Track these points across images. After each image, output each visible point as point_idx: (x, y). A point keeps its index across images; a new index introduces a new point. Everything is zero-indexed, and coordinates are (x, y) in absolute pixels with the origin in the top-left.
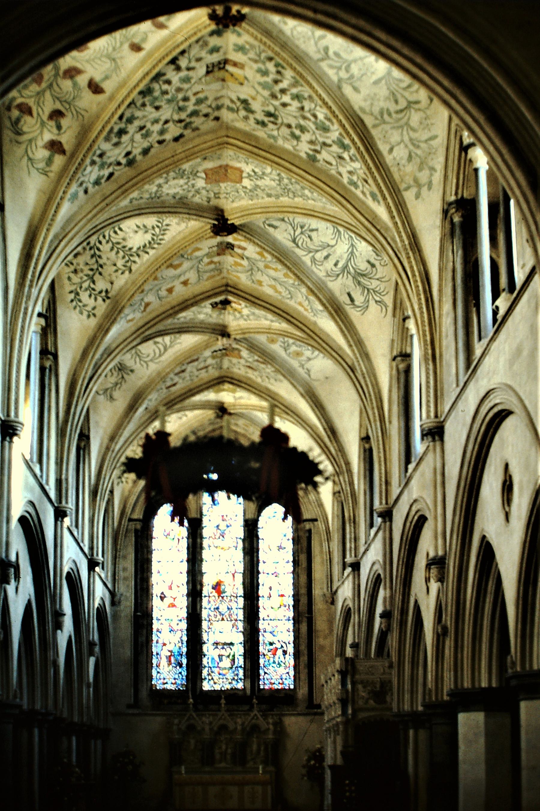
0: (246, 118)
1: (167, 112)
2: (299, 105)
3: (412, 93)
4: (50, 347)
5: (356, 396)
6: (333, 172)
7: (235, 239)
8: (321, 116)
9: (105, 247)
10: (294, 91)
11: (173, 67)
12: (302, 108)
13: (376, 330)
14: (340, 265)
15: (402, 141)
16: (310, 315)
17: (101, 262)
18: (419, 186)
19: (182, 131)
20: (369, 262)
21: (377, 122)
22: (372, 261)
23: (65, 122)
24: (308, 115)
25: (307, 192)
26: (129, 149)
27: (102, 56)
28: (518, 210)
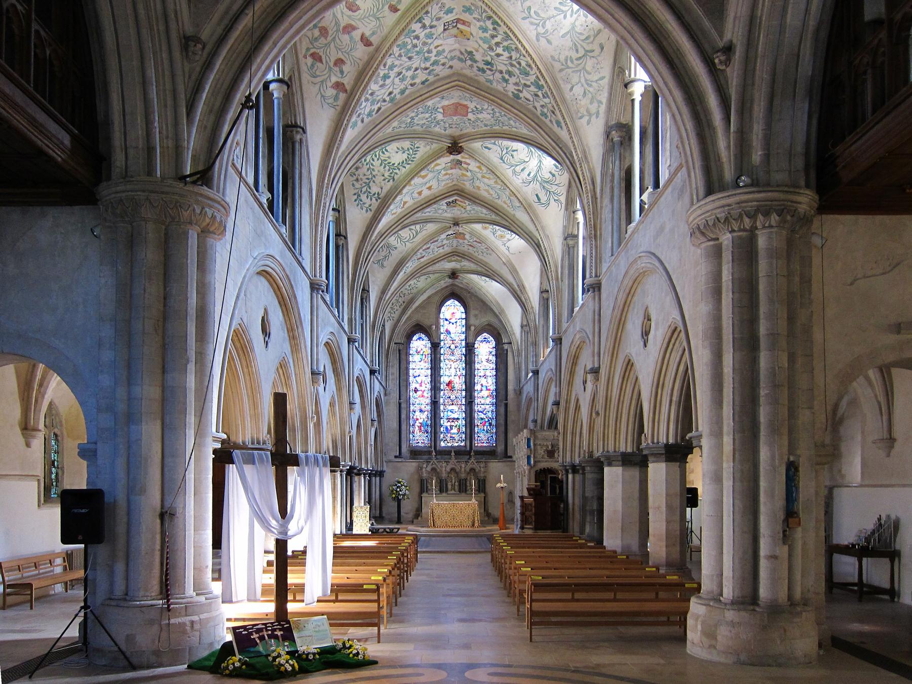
0: (471, 66)
1: (416, 63)
4: (343, 232)
5: (539, 264)
6: (530, 107)
7: (463, 157)
8: (523, 64)
10: (505, 44)
11: (420, 25)
12: (511, 58)
13: (553, 220)
15: (580, 81)
16: (510, 210)
17: (374, 173)
18: (590, 115)
20: (550, 173)
22: (553, 172)
23: (346, 68)
24: (514, 63)
25: (511, 122)
26: (391, 90)
28: (673, 123)
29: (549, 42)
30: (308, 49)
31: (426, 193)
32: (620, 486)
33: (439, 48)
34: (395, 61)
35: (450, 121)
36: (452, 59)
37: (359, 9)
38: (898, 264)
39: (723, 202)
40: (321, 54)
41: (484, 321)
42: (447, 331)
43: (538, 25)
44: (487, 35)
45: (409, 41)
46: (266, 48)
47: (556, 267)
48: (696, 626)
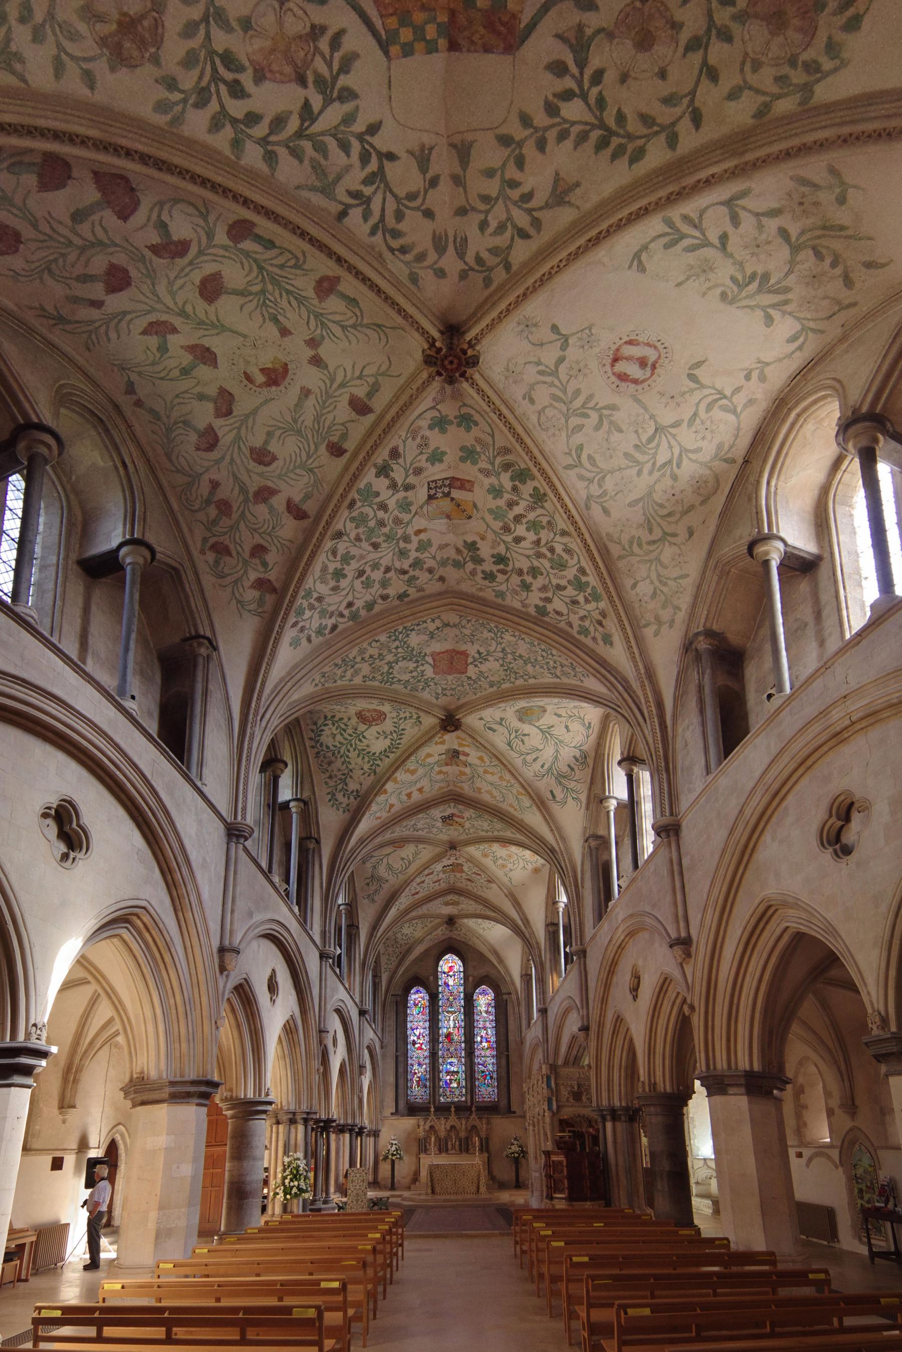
0: (473, 573)
1: (386, 556)
2: (535, 538)
3: (670, 523)
6: (563, 625)
8: (559, 549)
9: (353, 754)
10: (532, 516)
11: (387, 482)
12: (538, 542)
14: (546, 767)
15: (648, 577)
17: (350, 767)
19: (406, 588)
21: (624, 552)
24: (544, 550)
27: (295, 468)
29: (606, 511)
30: (205, 540)
31: (416, 797)
33: (423, 536)
37: (274, 458)
40: (227, 542)
41: (482, 972)
43: (591, 481)
44: (501, 502)
45: (371, 514)
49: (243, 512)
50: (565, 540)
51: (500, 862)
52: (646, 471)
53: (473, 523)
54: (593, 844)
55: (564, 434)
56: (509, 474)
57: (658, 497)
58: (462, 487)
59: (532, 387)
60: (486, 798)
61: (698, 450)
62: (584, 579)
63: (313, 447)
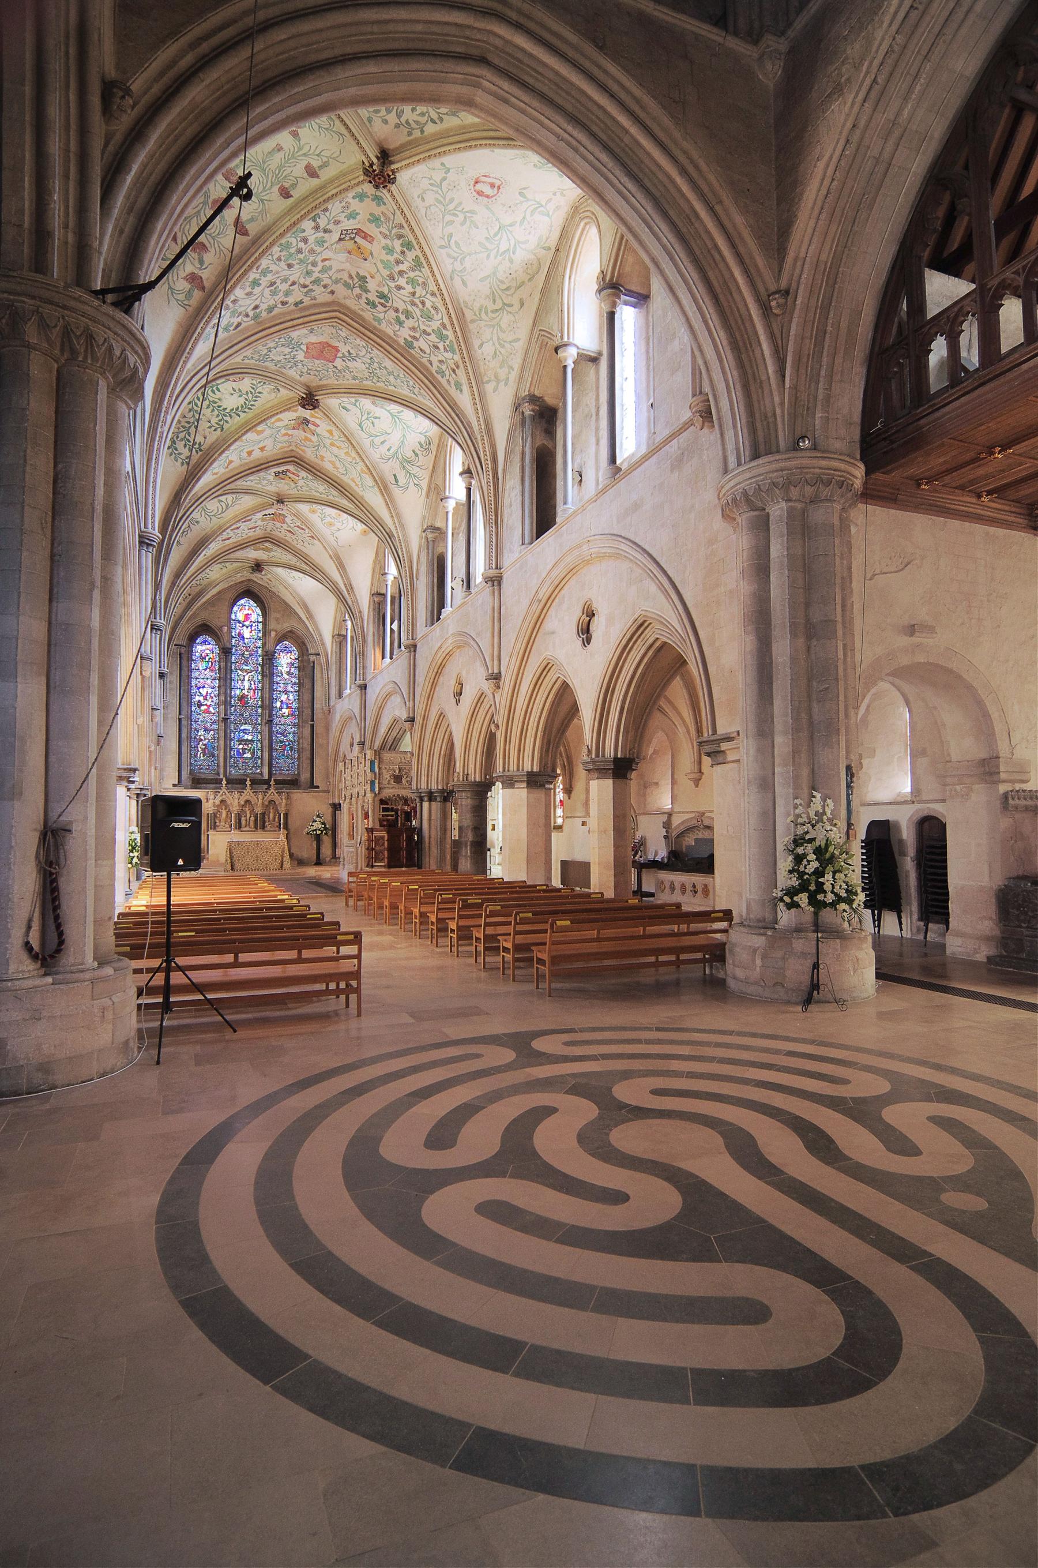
0: (359, 296)
1: (296, 274)
2: (412, 290)
6: (424, 361)
7: (312, 416)
8: (428, 304)
10: (411, 274)
11: (313, 224)
12: (414, 294)
15: (492, 338)
18: (498, 381)
22: (417, 451)
24: (417, 301)
26: (257, 303)
29: (464, 283)
31: (257, 454)
32: (524, 810)
33: (327, 263)
34: (270, 264)
35: (310, 365)
36: (337, 282)
38: (909, 563)
39: (782, 465)
42: (239, 634)
43: (456, 259)
44: (392, 259)
46: (220, 141)
47: (411, 562)
48: (754, 961)
49: (199, 212)
50: (433, 299)
51: (328, 519)
52: (492, 256)
53: (367, 264)
54: (430, 536)
55: (441, 225)
56: (401, 241)
57: (501, 275)
58: (365, 238)
59: (424, 192)
60: (327, 466)
61: (526, 242)
62: (445, 332)
63: (269, 184)
